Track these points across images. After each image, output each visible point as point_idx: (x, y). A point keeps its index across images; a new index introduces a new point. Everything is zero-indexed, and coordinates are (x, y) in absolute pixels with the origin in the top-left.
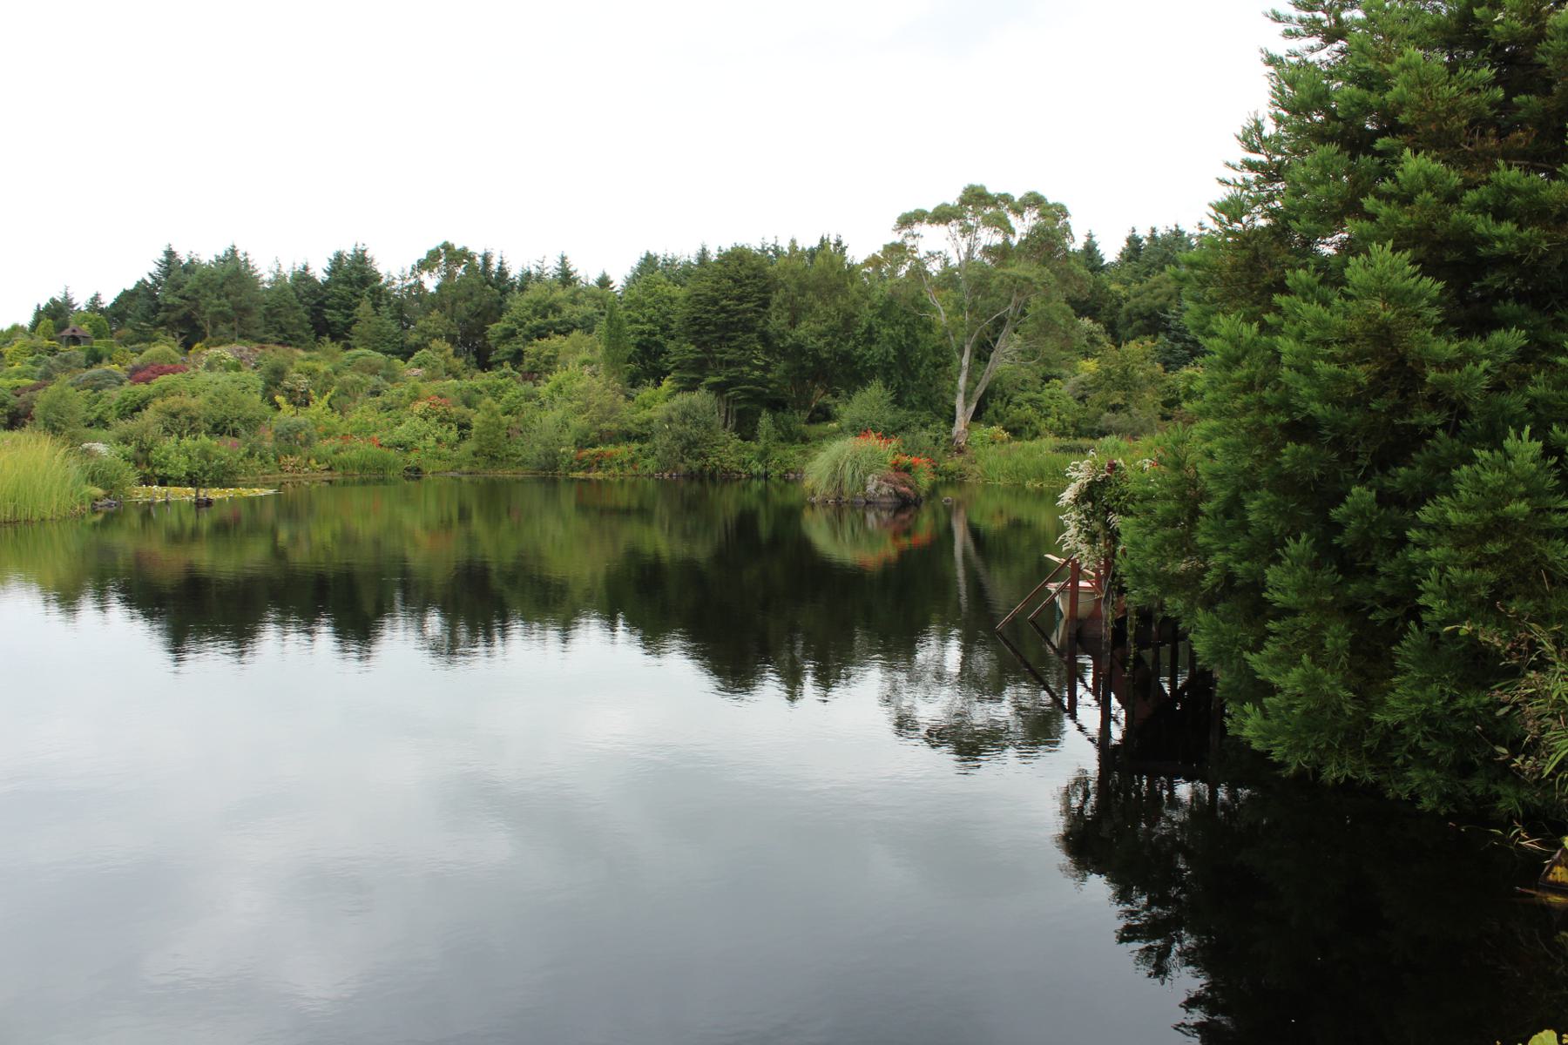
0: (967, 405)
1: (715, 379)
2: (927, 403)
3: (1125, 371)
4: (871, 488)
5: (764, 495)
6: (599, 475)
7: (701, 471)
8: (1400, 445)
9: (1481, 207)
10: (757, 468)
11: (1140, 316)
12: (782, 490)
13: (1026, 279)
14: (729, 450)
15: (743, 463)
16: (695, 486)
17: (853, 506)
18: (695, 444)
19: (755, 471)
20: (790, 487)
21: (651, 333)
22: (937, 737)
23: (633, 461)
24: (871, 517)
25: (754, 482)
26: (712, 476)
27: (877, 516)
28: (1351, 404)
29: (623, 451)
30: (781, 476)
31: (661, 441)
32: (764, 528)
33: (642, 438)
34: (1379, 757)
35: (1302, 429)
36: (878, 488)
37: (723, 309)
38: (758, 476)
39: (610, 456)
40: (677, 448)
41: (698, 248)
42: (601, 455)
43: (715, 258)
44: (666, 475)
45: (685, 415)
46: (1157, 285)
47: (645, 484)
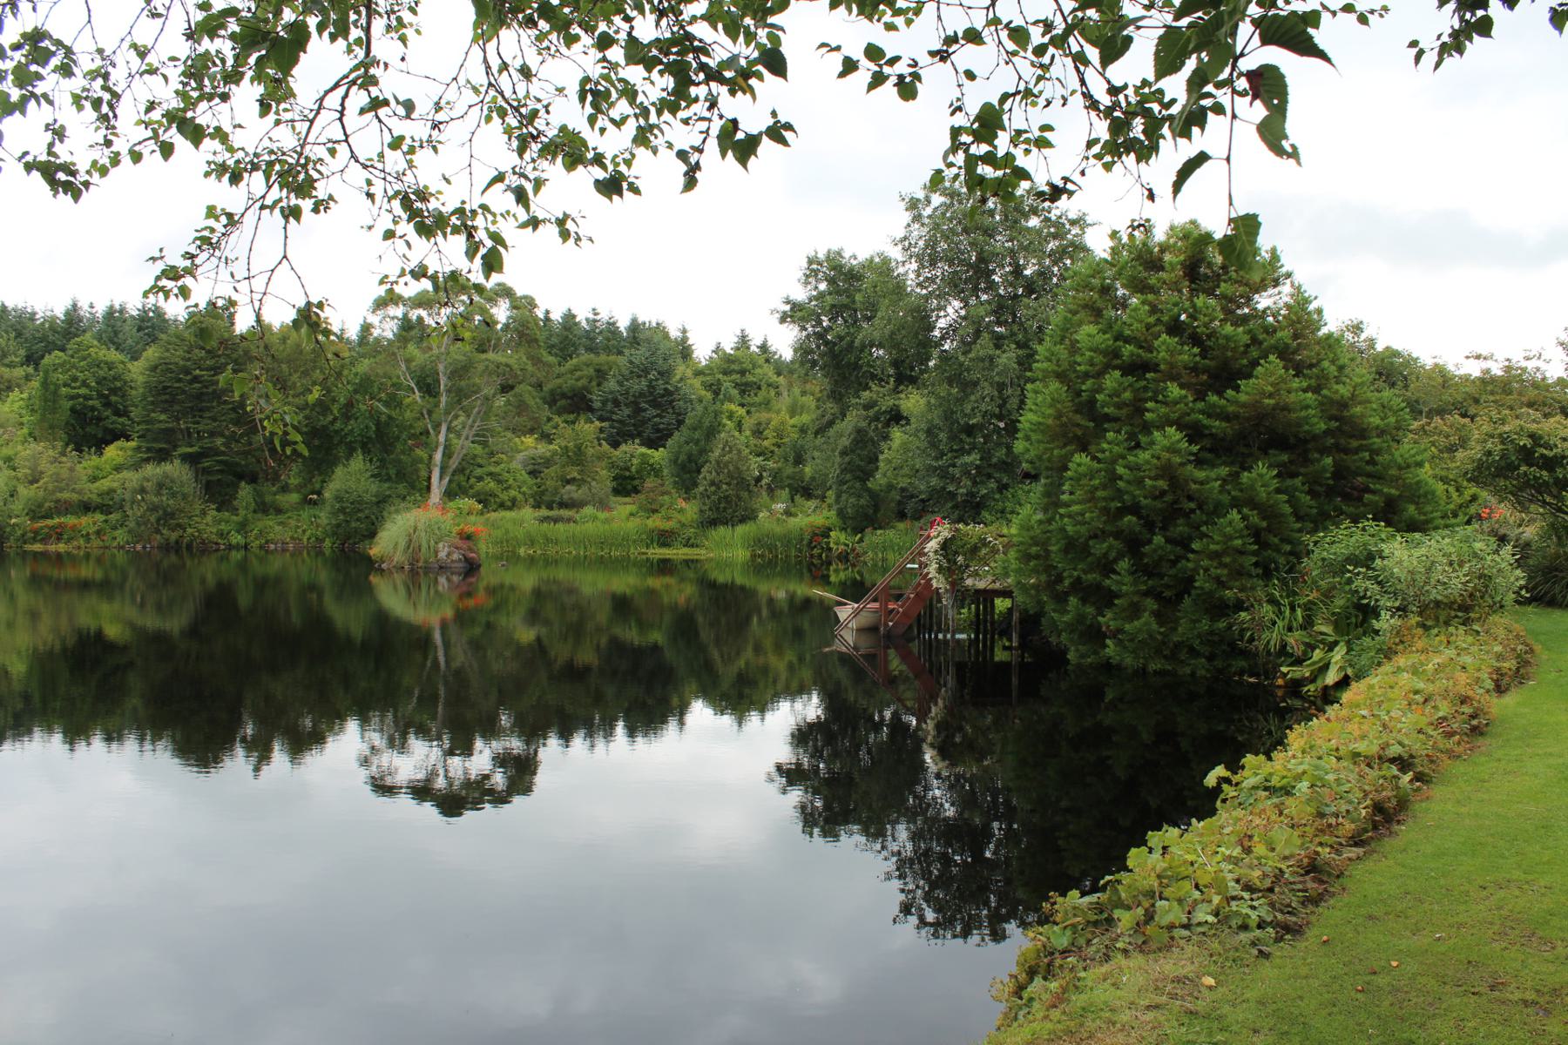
0: (441, 478)
1: (189, 450)
2: (401, 476)
3: (579, 447)
4: (442, 555)
5: (243, 566)
6: (61, 547)
7: (177, 542)
8: (1173, 513)
9: (1202, 412)
10: (236, 539)
11: (564, 396)
12: (261, 560)
13: (507, 365)
14: (208, 523)
15: (221, 534)
16: (167, 558)
17: (427, 570)
18: (172, 515)
19: (234, 542)
20: (271, 557)
21: (86, 398)
22: (421, 791)
23: (98, 533)
24: (442, 580)
25: (234, 553)
26: (189, 547)
27: (448, 580)
28: (1155, 498)
29: (88, 522)
30: (261, 547)
31: (134, 513)
32: (244, 599)
33: (105, 509)
34: (1173, 657)
35: (1134, 509)
36: (449, 554)
37: (196, 379)
38: (237, 547)
39: (73, 528)
40: (153, 519)
41: (68, 304)
42: (60, 525)
43: (238, 332)
44: (139, 547)
45: (160, 486)
46: (576, 369)
47: (114, 556)
